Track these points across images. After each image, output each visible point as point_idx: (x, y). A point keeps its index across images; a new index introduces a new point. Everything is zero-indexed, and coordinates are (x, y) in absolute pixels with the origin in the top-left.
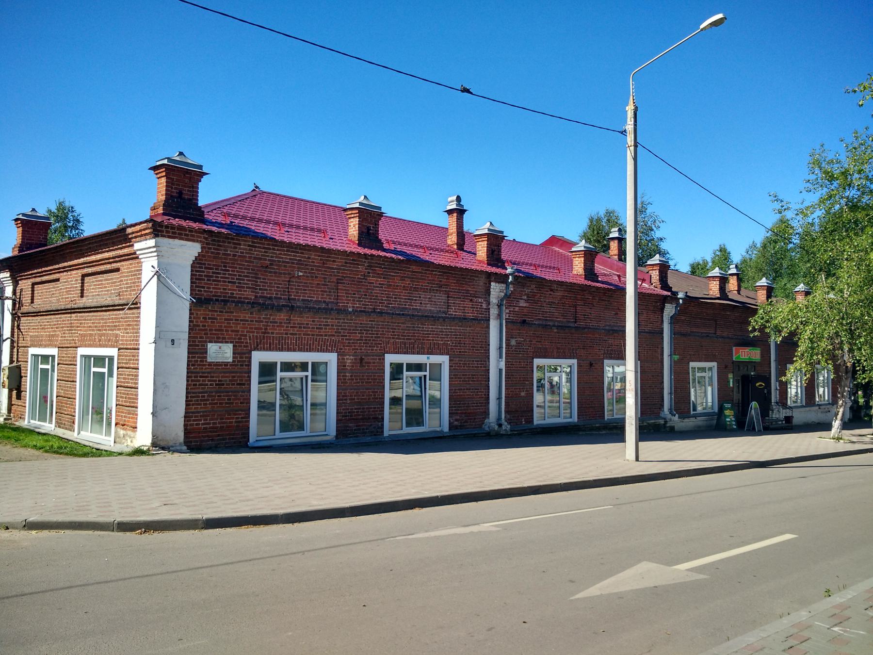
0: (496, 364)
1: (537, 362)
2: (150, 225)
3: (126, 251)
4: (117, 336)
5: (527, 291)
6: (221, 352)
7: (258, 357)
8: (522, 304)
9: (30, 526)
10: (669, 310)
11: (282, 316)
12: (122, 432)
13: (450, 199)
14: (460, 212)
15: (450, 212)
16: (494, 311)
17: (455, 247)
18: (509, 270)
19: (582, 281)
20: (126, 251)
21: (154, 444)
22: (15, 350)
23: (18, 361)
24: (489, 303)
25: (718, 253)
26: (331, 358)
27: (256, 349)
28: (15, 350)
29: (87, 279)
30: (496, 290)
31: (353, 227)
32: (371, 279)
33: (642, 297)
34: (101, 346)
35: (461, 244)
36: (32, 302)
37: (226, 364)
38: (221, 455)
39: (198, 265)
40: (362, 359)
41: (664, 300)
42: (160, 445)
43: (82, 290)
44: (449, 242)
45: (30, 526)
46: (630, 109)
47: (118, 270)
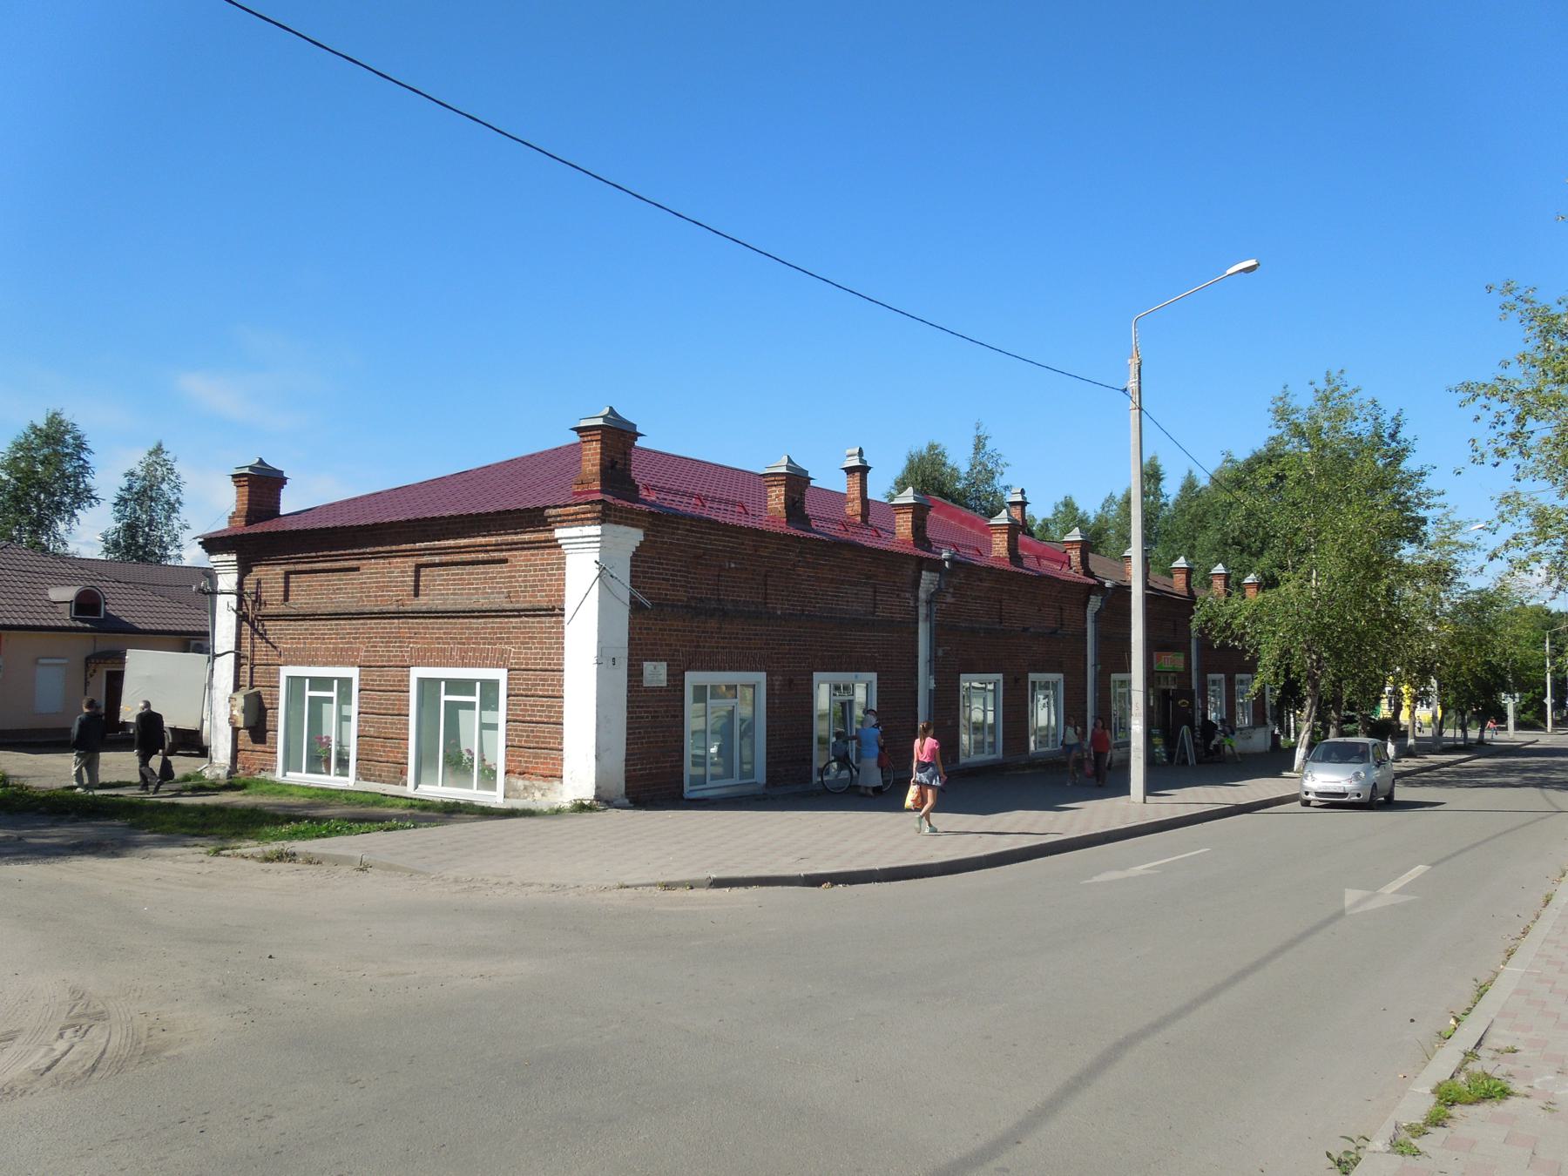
0: (925, 682)
1: (1032, 677)
2: (599, 507)
3: (542, 536)
4: (503, 652)
5: (956, 581)
6: (656, 673)
7: (692, 679)
8: (950, 599)
9: (719, 883)
10: (1095, 603)
11: (713, 624)
12: (520, 783)
13: (848, 452)
14: (862, 470)
15: (850, 471)
16: (922, 611)
17: (859, 518)
18: (945, 555)
19: (910, 550)
20: (542, 536)
21: (597, 797)
22: (246, 668)
23: (252, 686)
24: (917, 599)
25: (1062, 508)
26: (501, 675)
27: (689, 669)
28: (246, 668)
29: (424, 572)
30: (927, 579)
31: (776, 499)
32: (800, 570)
33: (1154, 599)
34: (464, 665)
35: (865, 514)
36: (286, 599)
37: (661, 689)
38: (103, 860)
39: (637, 558)
40: (791, 681)
41: (1090, 590)
42: (604, 800)
43: (417, 586)
44: (849, 511)
45: (719, 883)
46: (1133, 363)
47: (505, 561)
